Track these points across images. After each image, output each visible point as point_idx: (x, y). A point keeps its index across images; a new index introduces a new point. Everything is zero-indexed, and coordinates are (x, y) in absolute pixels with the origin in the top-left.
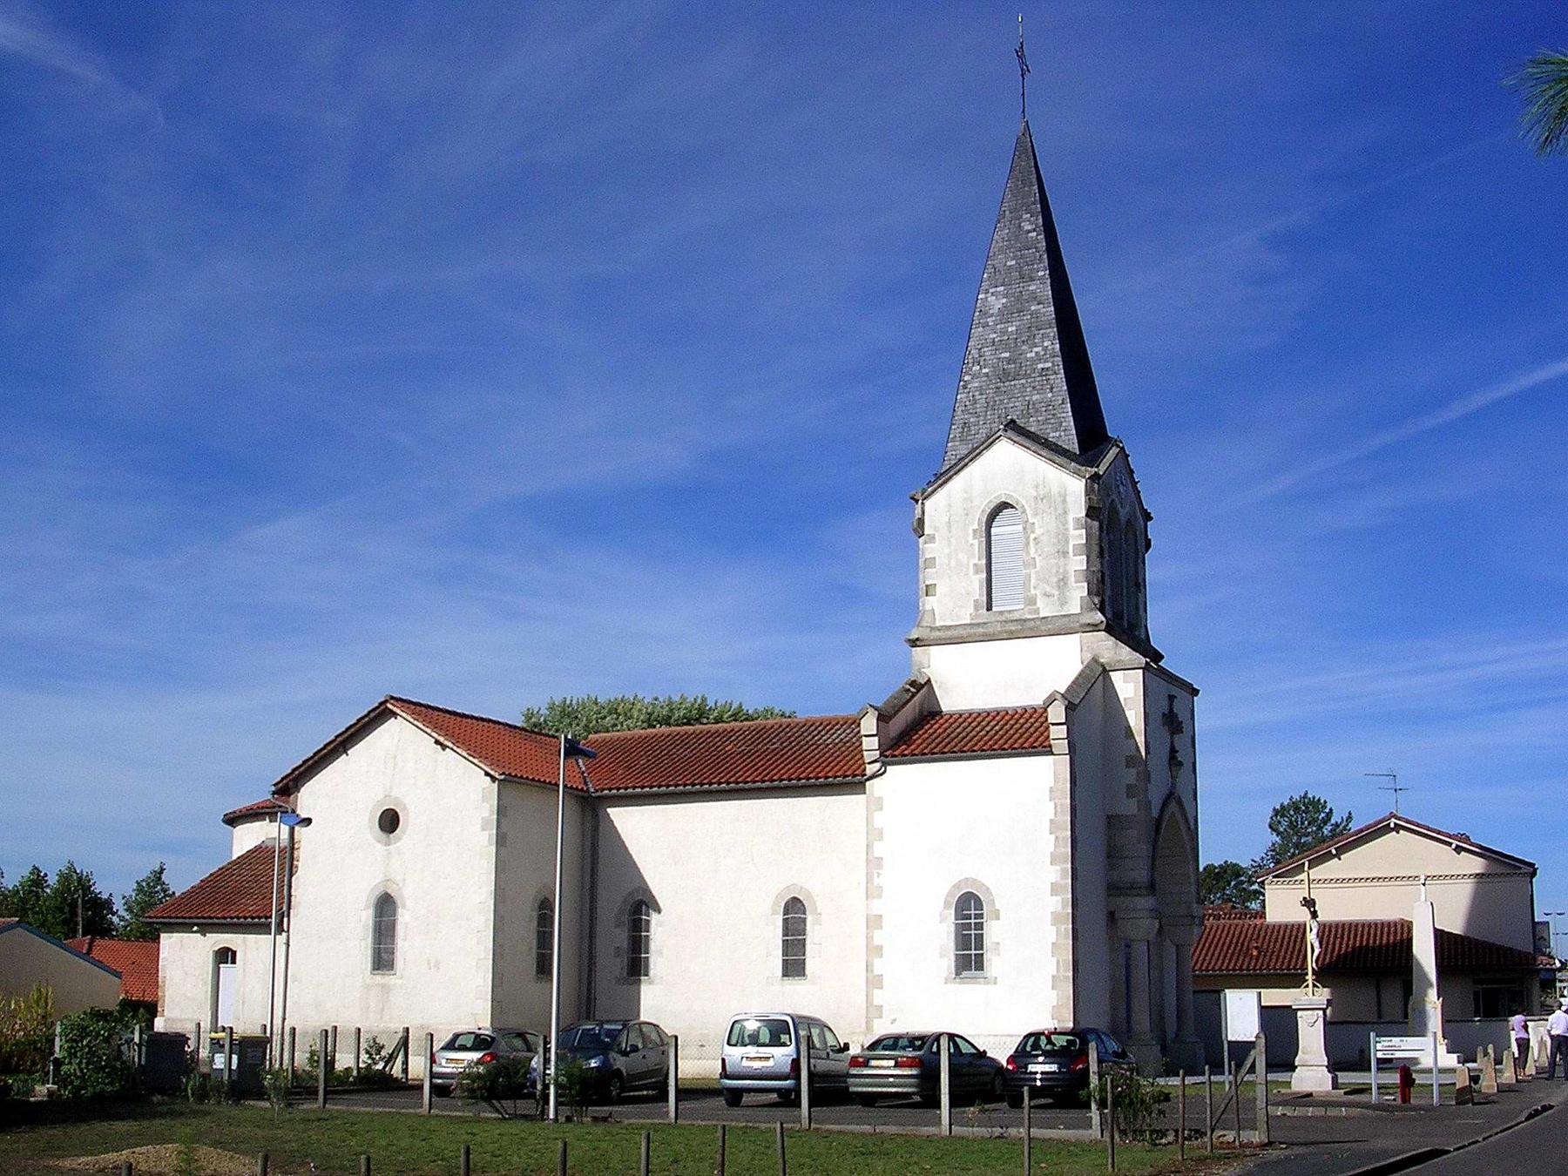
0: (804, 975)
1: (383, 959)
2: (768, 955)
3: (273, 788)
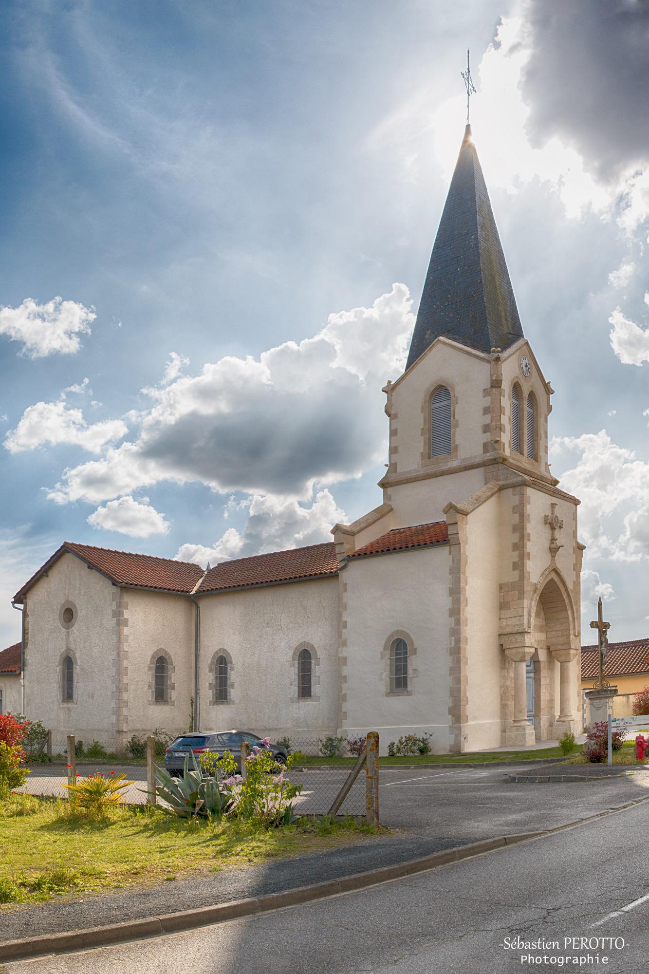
0: (310, 696)
1: (68, 695)
2: (291, 684)
3: (13, 600)
